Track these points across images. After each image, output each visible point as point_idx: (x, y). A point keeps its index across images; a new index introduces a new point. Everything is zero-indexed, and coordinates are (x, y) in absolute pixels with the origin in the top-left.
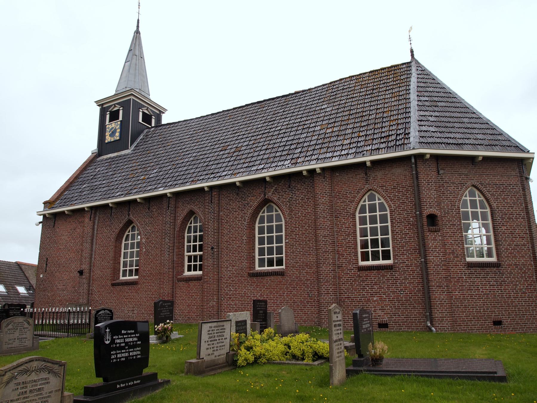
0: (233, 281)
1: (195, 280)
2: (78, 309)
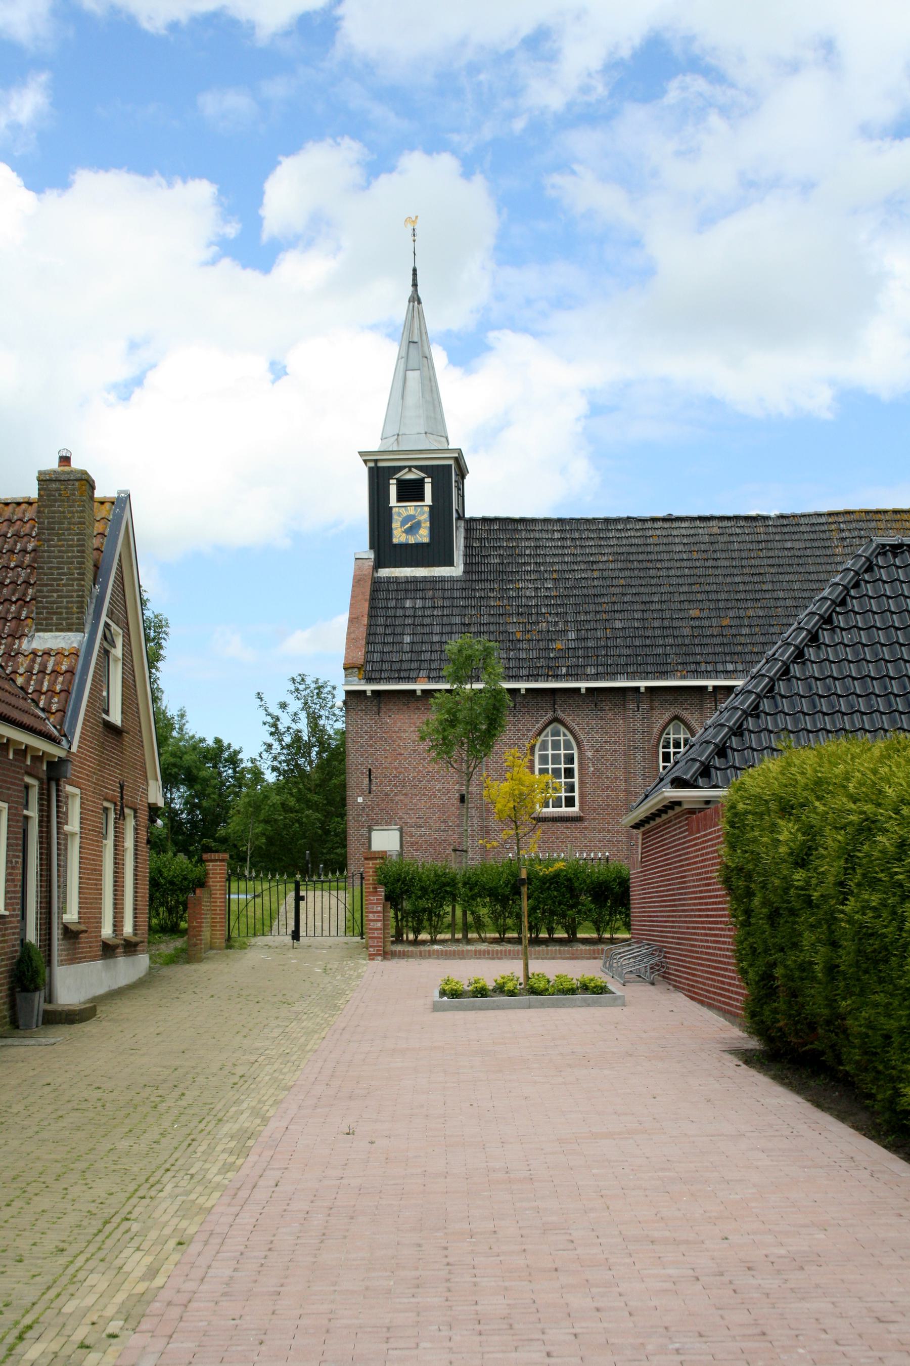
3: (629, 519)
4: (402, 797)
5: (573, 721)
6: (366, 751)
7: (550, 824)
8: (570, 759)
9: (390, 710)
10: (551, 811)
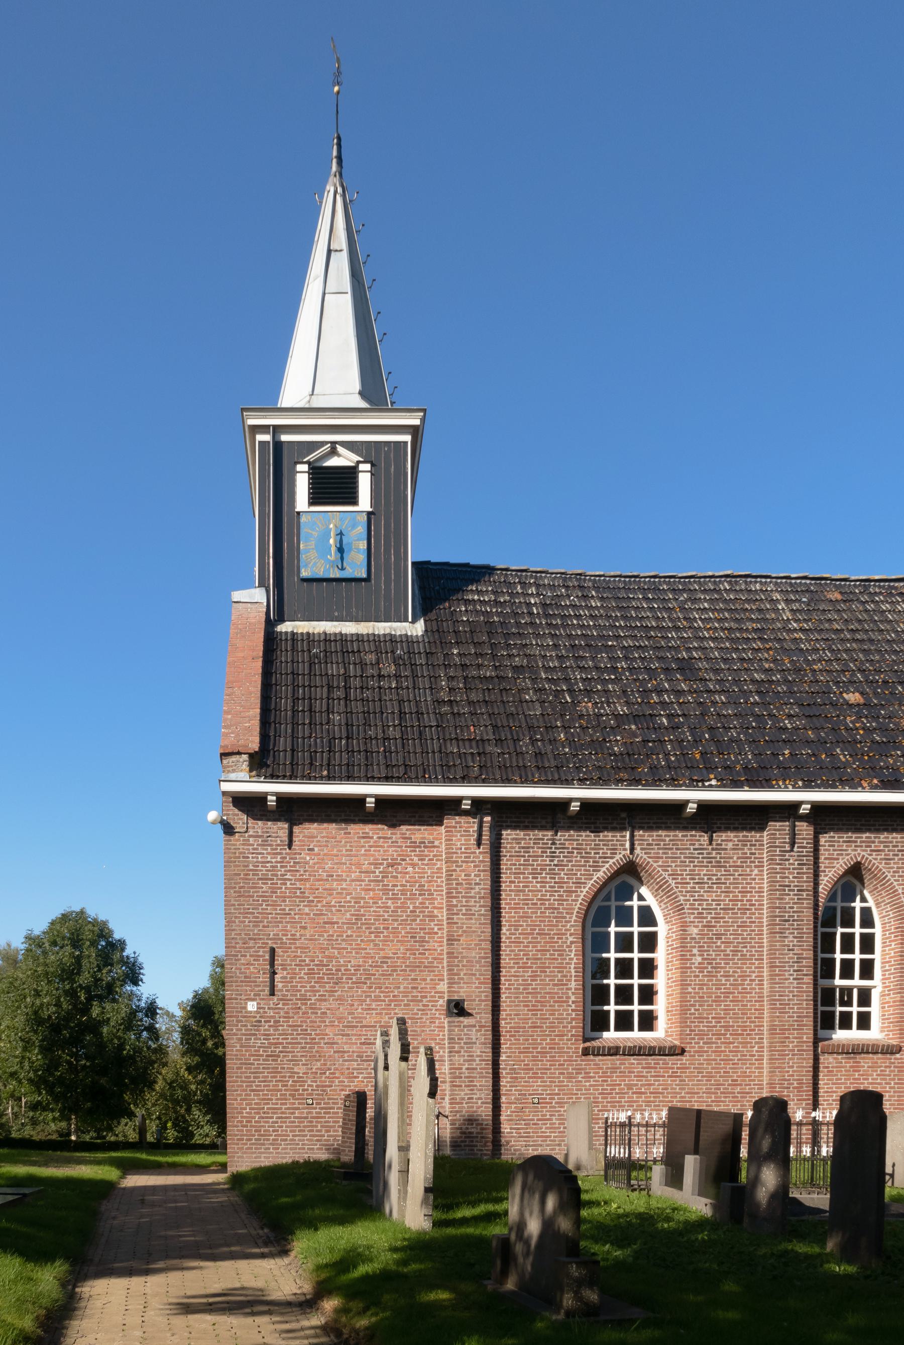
4: (334, 1005)
5: (665, 868)
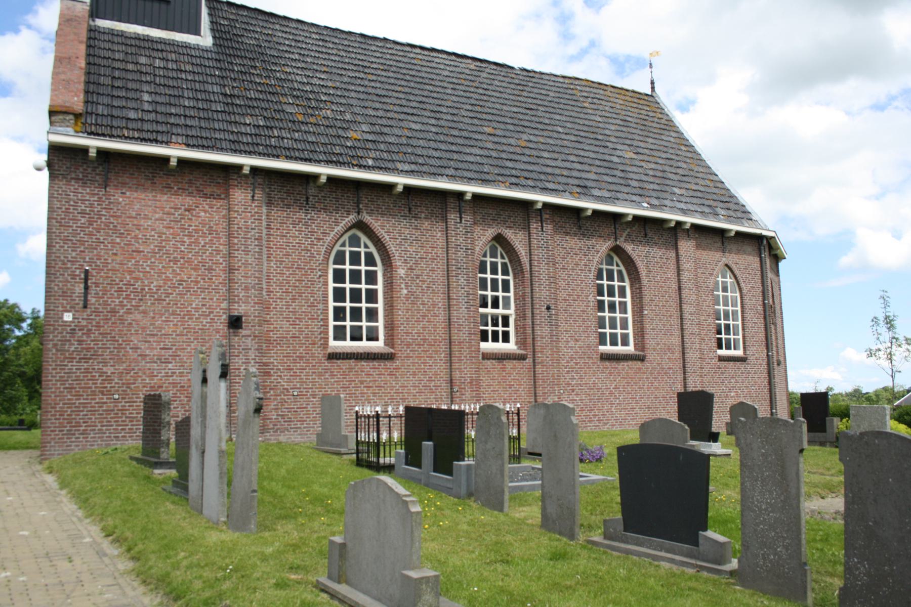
0: (576, 364)
1: (515, 359)
2: (472, 406)
3: (385, 40)
4: (139, 317)
6: (82, 242)
7: (352, 362)
8: (371, 278)
9: (124, 184)
10: (348, 345)
